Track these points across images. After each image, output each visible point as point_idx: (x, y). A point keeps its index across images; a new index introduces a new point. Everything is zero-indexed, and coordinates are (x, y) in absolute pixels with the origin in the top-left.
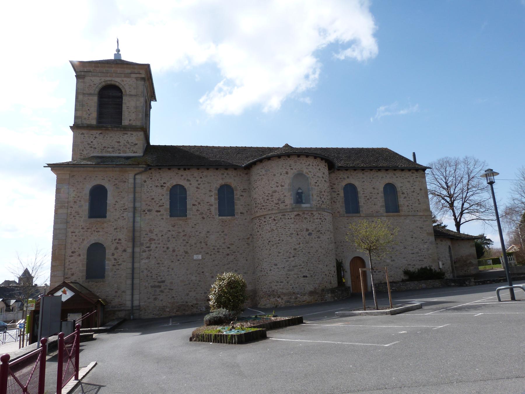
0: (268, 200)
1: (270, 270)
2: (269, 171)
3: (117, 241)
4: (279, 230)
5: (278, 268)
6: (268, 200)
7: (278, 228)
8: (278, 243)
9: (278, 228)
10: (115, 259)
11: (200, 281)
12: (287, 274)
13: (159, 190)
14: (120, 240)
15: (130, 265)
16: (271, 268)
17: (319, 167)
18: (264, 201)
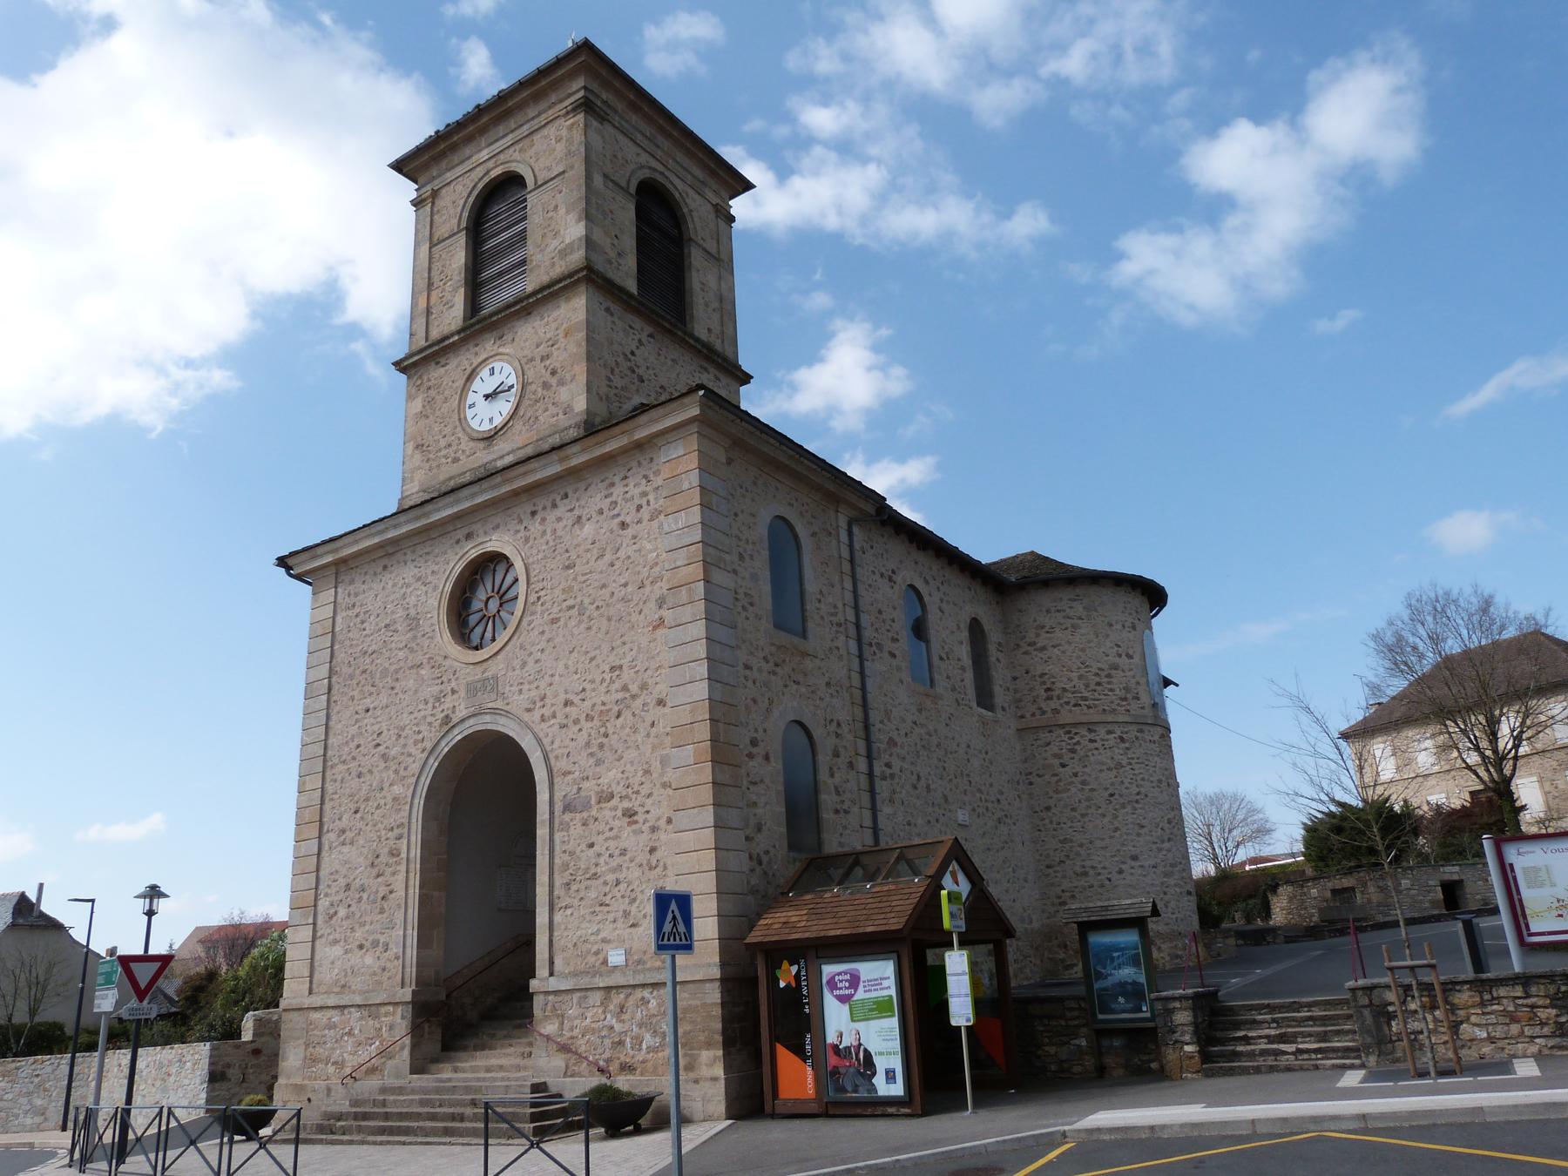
0: (1098, 684)
1: (1121, 872)
2: (1096, 610)
5: (1142, 866)
6: (1098, 684)
8: (1137, 801)
16: (1123, 866)
18: (1087, 686)
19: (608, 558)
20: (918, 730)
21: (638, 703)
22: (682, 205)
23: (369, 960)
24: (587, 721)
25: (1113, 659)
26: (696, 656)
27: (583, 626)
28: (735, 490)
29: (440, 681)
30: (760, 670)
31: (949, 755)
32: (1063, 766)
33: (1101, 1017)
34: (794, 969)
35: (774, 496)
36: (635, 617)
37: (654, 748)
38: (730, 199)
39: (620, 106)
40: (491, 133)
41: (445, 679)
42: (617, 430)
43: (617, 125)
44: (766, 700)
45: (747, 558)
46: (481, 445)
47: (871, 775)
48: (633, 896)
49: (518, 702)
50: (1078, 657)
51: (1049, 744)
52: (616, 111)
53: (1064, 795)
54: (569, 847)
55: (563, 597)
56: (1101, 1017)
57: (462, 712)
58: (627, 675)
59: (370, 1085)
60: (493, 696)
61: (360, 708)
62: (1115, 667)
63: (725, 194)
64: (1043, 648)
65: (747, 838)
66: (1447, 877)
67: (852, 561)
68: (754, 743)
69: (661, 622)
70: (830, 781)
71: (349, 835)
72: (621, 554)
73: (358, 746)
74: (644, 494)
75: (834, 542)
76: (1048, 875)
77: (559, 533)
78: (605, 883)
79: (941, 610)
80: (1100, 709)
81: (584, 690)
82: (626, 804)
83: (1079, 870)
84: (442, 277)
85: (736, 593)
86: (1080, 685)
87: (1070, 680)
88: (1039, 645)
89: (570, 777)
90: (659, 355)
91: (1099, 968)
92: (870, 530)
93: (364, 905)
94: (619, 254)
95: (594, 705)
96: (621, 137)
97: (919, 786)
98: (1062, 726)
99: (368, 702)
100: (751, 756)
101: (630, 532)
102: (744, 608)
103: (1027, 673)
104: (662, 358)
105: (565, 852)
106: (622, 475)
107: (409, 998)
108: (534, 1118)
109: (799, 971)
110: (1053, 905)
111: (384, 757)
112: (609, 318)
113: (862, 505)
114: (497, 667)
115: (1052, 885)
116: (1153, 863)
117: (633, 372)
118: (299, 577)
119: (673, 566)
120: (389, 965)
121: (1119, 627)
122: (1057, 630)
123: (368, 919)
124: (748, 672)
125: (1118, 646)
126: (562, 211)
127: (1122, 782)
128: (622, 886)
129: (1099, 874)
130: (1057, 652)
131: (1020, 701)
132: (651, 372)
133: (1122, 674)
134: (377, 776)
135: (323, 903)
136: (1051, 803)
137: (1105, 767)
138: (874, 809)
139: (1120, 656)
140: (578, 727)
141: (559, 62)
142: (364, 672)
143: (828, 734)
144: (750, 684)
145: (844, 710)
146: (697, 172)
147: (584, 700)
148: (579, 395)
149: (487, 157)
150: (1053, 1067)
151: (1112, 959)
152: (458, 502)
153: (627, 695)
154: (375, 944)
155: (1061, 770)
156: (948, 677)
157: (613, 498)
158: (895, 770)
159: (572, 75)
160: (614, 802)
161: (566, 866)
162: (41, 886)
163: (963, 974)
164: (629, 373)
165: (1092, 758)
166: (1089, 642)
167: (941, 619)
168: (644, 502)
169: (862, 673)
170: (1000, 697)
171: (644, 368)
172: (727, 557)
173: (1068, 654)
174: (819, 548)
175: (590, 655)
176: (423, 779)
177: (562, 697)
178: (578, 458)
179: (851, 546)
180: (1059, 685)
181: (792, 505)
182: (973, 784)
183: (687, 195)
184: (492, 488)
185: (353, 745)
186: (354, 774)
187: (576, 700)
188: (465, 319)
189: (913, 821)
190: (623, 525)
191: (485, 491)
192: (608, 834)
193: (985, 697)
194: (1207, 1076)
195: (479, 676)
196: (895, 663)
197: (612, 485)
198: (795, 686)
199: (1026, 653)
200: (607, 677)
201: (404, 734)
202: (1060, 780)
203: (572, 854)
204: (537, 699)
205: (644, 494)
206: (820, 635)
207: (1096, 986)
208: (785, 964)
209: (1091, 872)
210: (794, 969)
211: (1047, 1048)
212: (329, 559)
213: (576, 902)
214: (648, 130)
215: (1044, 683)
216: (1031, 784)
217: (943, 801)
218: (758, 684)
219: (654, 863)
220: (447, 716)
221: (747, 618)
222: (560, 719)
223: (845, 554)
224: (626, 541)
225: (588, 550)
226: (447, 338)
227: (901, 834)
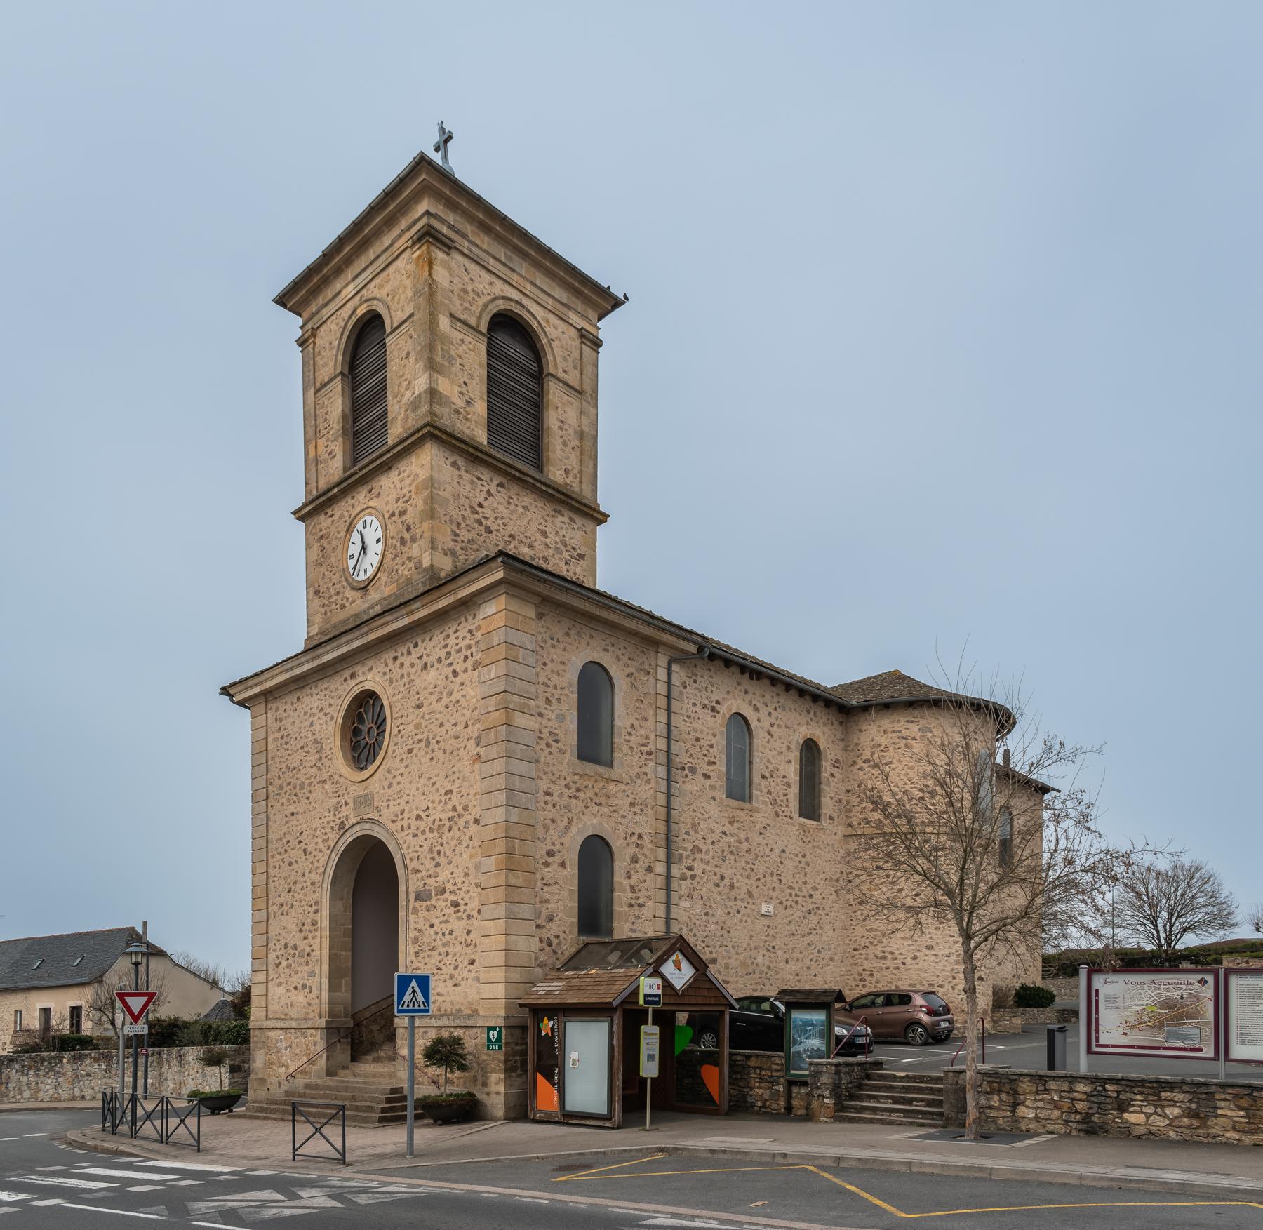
1: (915, 958)
2: (931, 732)
3: (635, 838)
5: (935, 955)
10: (633, 890)
11: (769, 968)
12: (953, 970)
13: (706, 716)
14: (640, 837)
15: (661, 912)
16: (918, 954)
19: (445, 701)
20: (726, 839)
21: (461, 822)
22: (542, 335)
23: (301, 998)
26: (498, 787)
27: (429, 757)
28: (546, 642)
30: (561, 795)
31: (759, 859)
33: (792, 1072)
34: (551, 1023)
35: (588, 644)
37: (471, 856)
39: (469, 229)
41: (340, 793)
42: (445, 590)
43: (466, 251)
44: (566, 819)
45: (554, 701)
46: (359, 594)
47: (668, 877)
48: (456, 964)
49: (386, 817)
52: (464, 236)
54: (418, 927)
55: (416, 732)
56: (792, 1072)
57: (352, 821)
58: (455, 797)
59: (300, 1081)
60: (371, 809)
61: (288, 813)
63: (592, 315)
65: (538, 927)
67: (668, 697)
68: (550, 853)
70: (626, 882)
71: (285, 908)
72: (453, 698)
73: (288, 842)
74: (469, 647)
75: (652, 680)
76: (853, 957)
77: (412, 677)
78: (440, 954)
79: (769, 733)
81: (428, 808)
82: (453, 898)
83: (879, 954)
85: (541, 732)
90: (509, 503)
92: (696, 666)
93: (296, 958)
94: (468, 402)
95: (434, 821)
96: (472, 267)
97: (722, 885)
99: (292, 808)
100: (546, 864)
101: (458, 680)
102: (548, 745)
104: (512, 507)
106: (453, 629)
107: (324, 1025)
108: (384, 1110)
109: (553, 1025)
110: (854, 980)
112: (456, 472)
113: (683, 645)
115: (856, 964)
116: (947, 953)
117: (481, 524)
118: (241, 703)
120: (312, 1002)
122: (891, 749)
123: (299, 969)
124: (548, 798)
126: (412, 359)
128: (450, 957)
129: (896, 959)
132: (500, 522)
134: (301, 864)
135: (272, 956)
138: (668, 904)
140: (424, 837)
142: (289, 784)
143: (628, 845)
144: (550, 807)
145: (648, 825)
146: (559, 293)
150: (759, 1104)
151: (806, 1032)
152: (339, 646)
154: (304, 987)
156: (769, 793)
158: (698, 872)
159: (416, 197)
160: (447, 895)
161: (416, 940)
162: (145, 923)
163: (655, 1034)
164: (476, 525)
167: (768, 742)
169: (669, 795)
170: (828, 805)
171: (492, 519)
172: (532, 703)
174: (634, 686)
175: (432, 781)
176: (328, 869)
177: (415, 813)
179: (669, 683)
181: (608, 650)
182: (784, 882)
183: (548, 322)
185: (284, 841)
186: (287, 862)
187: (423, 815)
188: (345, 470)
189: (711, 912)
191: (357, 638)
192: (442, 919)
193: (810, 807)
194: (835, 1121)
196: (708, 782)
198: (597, 808)
199: (860, 769)
203: (420, 931)
204: (399, 813)
206: (627, 759)
207: (792, 1050)
208: (546, 1019)
209: (889, 957)
210: (551, 1023)
212: (257, 690)
214: (501, 253)
217: (747, 896)
218: (557, 807)
219: (469, 942)
220: (342, 822)
221: (550, 753)
223: (662, 689)
224: (457, 687)
227: (697, 923)
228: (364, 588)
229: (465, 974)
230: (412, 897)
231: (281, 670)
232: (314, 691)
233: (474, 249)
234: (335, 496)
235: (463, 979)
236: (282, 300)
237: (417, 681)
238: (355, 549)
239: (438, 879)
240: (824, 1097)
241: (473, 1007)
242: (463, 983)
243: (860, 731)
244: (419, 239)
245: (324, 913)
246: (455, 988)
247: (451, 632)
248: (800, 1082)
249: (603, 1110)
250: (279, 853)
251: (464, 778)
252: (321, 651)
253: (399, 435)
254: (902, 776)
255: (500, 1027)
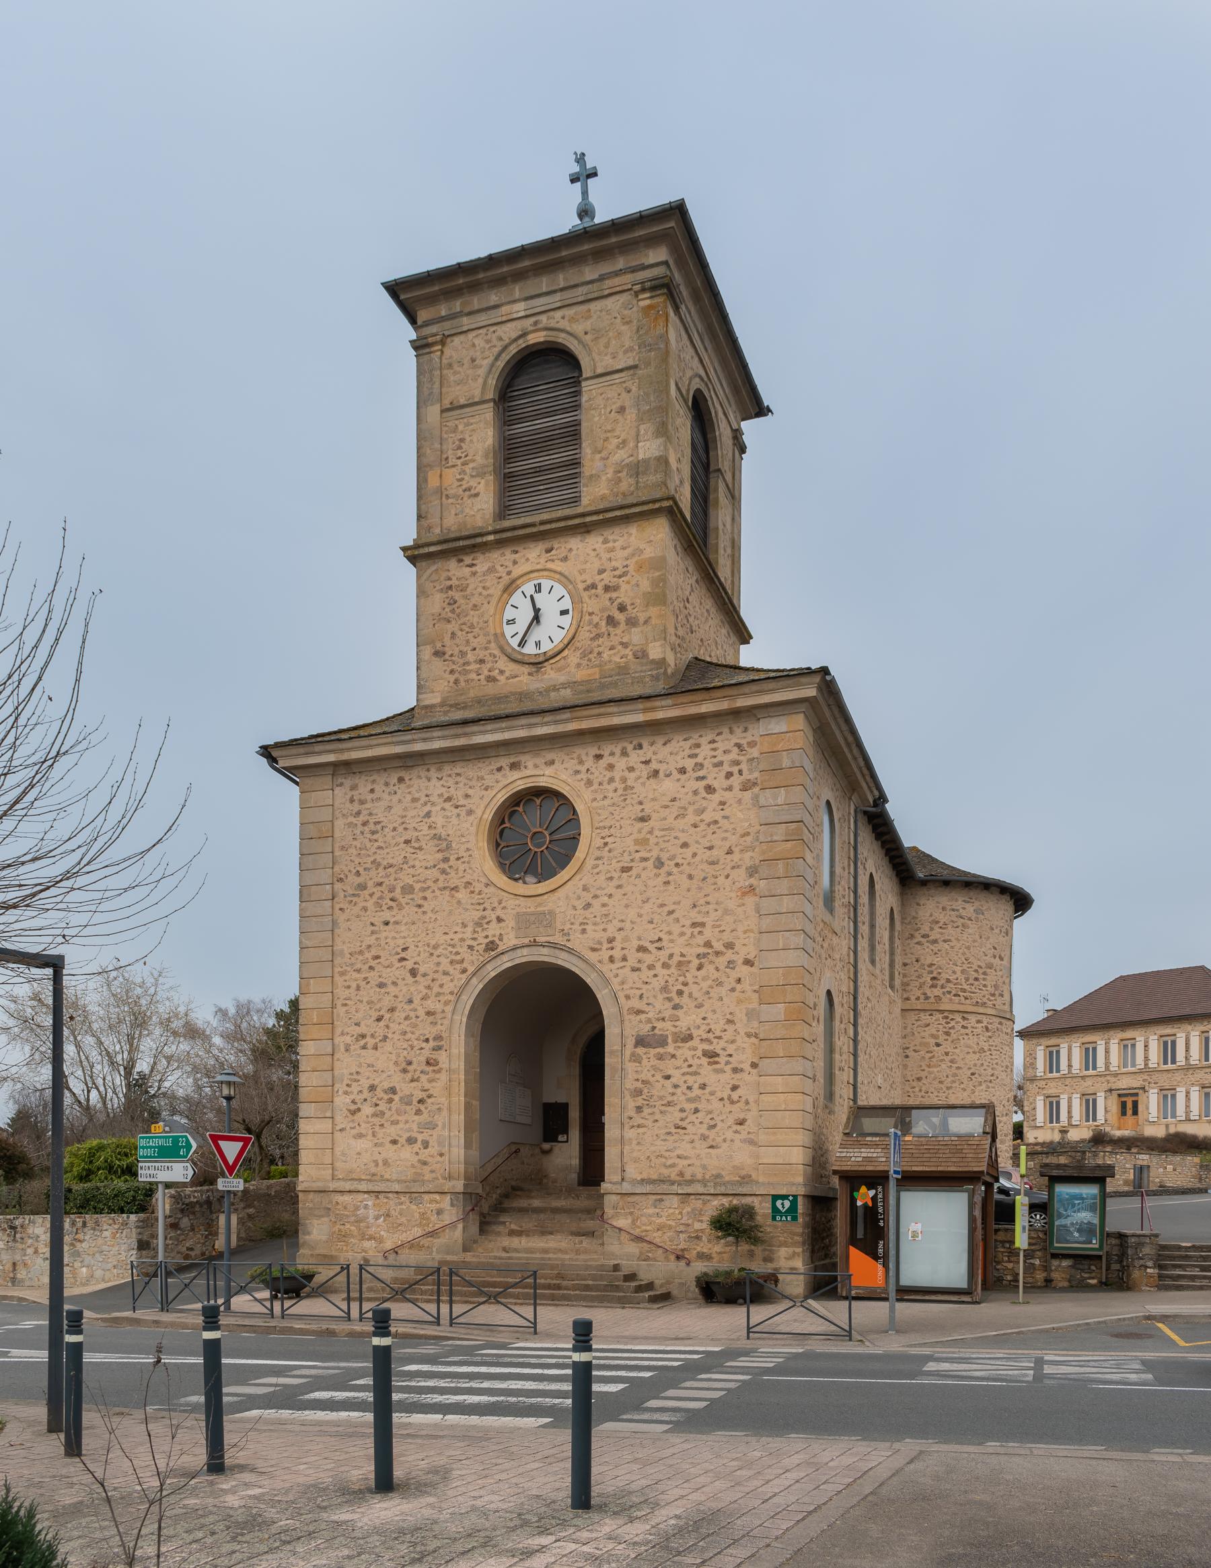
0: (976, 979)
2: (983, 914)
4: (994, 1053)
6: (976, 979)
7: (992, 1048)
8: (991, 1082)
9: (992, 1048)
17: (451, 858)
18: (967, 979)
19: (691, 818)
24: (663, 967)
25: (989, 959)
29: (481, 907)
32: (938, 1045)
33: (1056, 1245)
34: (872, 1193)
36: (721, 880)
38: (743, 420)
40: (529, 282)
46: (526, 669)
49: (578, 942)
50: (964, 954)
51: (928, 1025)
53: (935, 1070)
57: (510, 940)
58: (708, 933)
62: (990, 966)
64: (935, 941)
66: (1140, 1163)
69: (752, 889)
80: (974, 1001)
84: (459, 453)
86: (962, 978)
87: (954, 972)
88: (931, 938)
89: (643, 1016)
91: (1062, 1210)
98: (942, 1011)
101: (716, 797)
103: (917, 961)
105: (637, 1080)
106: (710, 738)
109: (876, 1194)
111: (413, 973)
114: (550, 903)
119: (769, 839)
121: (997, 931)
125: (995, 948)
127: (982, 1065)
130: (947, 947)
131: (908, 985)
133: (994, 973)
136: (923, 1074)
137: (971, 1051)
139: (995, 957)
141: (641, 219)
147: (660, 949)
148: (655, 640)
149: (522, 314)
150: (1009, 1278)
151: (1074, 1205)
152: (509, 729)
153: (710, 951)
155: (935, 1048)
157: (699, 760)
159: (651, 241)
160: (695, 1042)
165: (962, 1041)
166: (974, 941)
168: (735, 769)
173: (956, 949)
177: (635, 943)
178: (666, 711)
180: (944, 976)
184: (556, 722)
187: (651, 947)
190: (710, 789)
191: (547, 724)
195: (532, 909)
197: (698, 746)
199: (918, 943)
200: (688, 931)
201: (437, 953)
202: (933, 1057)
205: (737, 763)
207: (1057, 1223)
208: (863, 1189)
211: (1005, 1264)
213: (649, 1123)
215: (931, 972)
216: (907, 1057)
222: (632, 962)
225: (666, 807)
226: (481, 535)
228: (537, 664)
229: (729, 1135)
230: (630, 1042)
231: (389, 740)
232: (433, 773)
233: (688, 316)
234: (485, 544)
235: (725, 1140)
236: (395, 289)
237: (638, 788)
238: (524, 615)
239: (677, 1023)
240: (1147, 1267)
241: (743, 1173)
242: (725, 1145)
243: (918, 904)
244: (653, 288)
245: (455, 1051)
246: (710, 1150)
247: (704, 741)
248: (1062, 1255)
249: (963, 1284)
250: (359, 971)
251: (726, 912)
252: (475, 728)
253: (603, 498)
254: (960, 955)
255: (795, 1197)
